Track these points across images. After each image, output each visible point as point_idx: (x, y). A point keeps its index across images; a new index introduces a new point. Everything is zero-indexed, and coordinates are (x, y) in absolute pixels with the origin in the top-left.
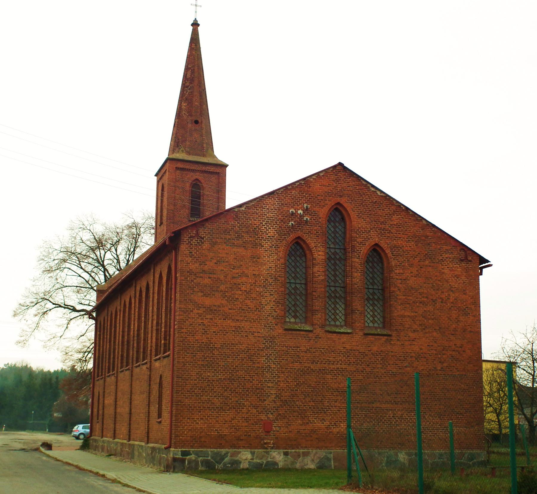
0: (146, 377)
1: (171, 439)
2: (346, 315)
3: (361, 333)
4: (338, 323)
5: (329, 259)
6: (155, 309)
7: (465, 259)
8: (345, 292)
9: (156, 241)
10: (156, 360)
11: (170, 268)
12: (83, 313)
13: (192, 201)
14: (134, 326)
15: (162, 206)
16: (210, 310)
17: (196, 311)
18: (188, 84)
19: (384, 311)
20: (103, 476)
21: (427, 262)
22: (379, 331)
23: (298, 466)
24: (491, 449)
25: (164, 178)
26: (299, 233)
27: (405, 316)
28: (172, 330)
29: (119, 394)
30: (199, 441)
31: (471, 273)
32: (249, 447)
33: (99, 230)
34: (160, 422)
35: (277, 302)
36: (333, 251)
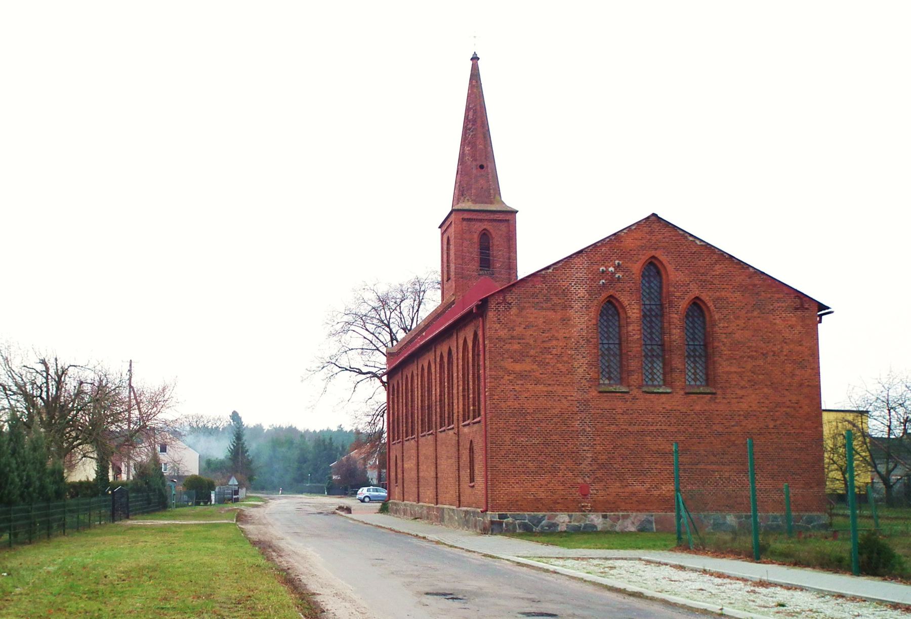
0: (454, 442)
1: (487, 502)
2: (664, 374)
3: (682, 392)
4: (656, 383)
5: (644, 316)
6: (461, 375)
7: (801, 308)
8: (663, 350)
9: (443, 300)
10: (464, 426)
11: (476, 335)
12: (369, 375)
13: (481, 253)
14: (436, 391)
15: (448, 261)
16: (521, 376)
17: (506, 377)
18: (470, 126)
19: (707, 368)
20: (424, 538)
21: (755, 313)
22: (701, 389)
23: (617, 529)
24: (835, 511)
25: (449, 230)
26: (611, 292)
27: (731, 373)
28: (482, 396)
29: (422, 458)
30: (515, 504)
31: (808, 322)
32: (566, 511)
33: (382, 290)
34: (473, 487)
35: (590, 364)
36: (648, 307)
